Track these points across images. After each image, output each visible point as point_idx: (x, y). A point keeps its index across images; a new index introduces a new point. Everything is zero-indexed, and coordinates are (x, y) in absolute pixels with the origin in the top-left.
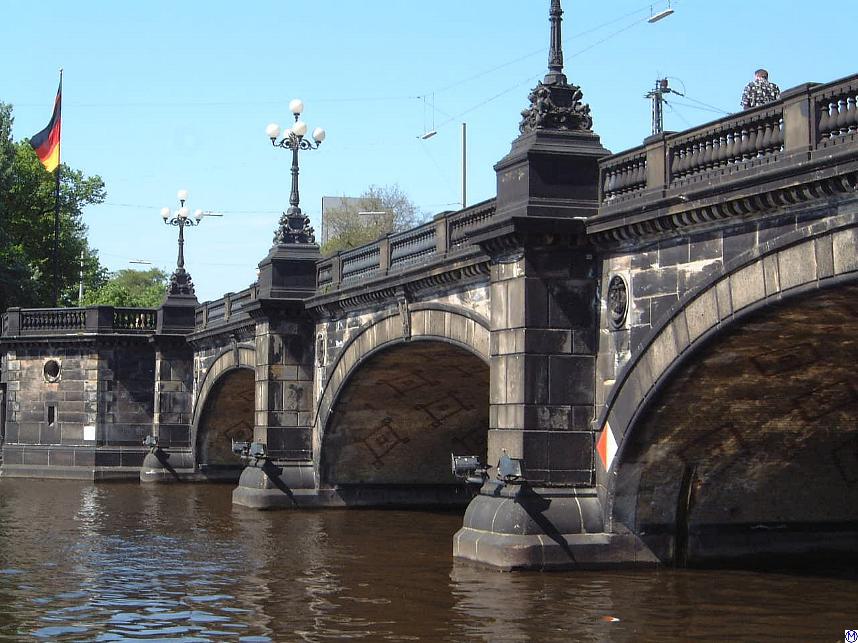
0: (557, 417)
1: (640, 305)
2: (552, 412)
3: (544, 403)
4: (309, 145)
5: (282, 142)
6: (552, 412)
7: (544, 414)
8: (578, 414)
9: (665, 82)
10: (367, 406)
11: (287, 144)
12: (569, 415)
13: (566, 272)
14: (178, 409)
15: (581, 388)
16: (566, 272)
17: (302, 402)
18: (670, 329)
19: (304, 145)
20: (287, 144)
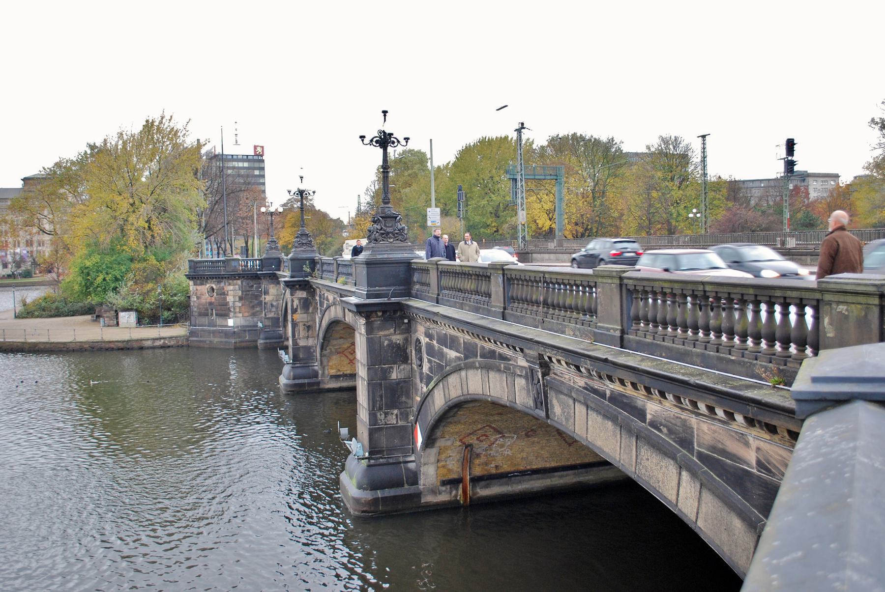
0: (389, 417)
1: (430, 361)
2: (386, 414)
3: (380, 409)
4: (398, 142)
5: (372, 141)
6: (386, 414)
7: (381, 416)
8: (401, 414)
9: (522, 124)
10: (341, 338)
11: (377, 142)
12: (397, 415)
13: (392, 330)
14: (274, 309)
15: (404, 399)
16: (392, 330)
17: (310, 332)
18: (441, 384)
19: (393, 143)
20: (377, 142)
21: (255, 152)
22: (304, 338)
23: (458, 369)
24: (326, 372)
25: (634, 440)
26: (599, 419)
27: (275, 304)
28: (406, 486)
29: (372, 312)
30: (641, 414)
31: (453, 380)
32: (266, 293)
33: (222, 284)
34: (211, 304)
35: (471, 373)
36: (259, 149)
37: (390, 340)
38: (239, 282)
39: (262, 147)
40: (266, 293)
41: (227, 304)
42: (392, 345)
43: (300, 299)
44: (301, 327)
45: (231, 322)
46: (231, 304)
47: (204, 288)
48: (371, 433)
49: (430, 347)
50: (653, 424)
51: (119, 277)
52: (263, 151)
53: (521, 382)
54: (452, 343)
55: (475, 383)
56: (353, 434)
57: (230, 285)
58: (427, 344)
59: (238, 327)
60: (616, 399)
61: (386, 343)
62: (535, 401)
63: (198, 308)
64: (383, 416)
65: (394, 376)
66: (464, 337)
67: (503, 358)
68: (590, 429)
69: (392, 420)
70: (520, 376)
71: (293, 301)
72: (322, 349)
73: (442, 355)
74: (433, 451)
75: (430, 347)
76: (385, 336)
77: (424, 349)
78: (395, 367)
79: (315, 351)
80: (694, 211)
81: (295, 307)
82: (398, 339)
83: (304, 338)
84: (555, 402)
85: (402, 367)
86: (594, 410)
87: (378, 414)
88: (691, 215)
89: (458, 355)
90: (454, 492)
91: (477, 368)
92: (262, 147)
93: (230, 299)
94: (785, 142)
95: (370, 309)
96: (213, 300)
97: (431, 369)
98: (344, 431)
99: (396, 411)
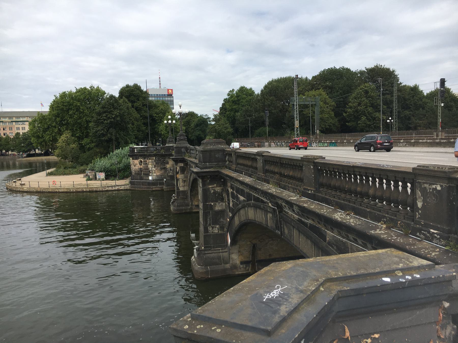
1: (233, 201)
2: (213, 228)
3: (210, 225)
7: (210, 229)
13: (215, 185)
15: (222, 220)
17: (185, 184)
21: (168, 92)
22: (182, 186)
23: (244, 207)
24: (193, 203)
25: (321, 251)
26: (305, 238)
27: (172, 168)
28: (223, 265)
29: (205, 176)
30: (323, 237)
31: (242, 212)
32: (168, 163)
33: (146, 160)
34: (141, 169)
35: (249, 209)
36: (170, 91)
37: (214, 190)
38: (154, 158)
39: (172, 90)
40: (168, 163)
41: (148, 169)
42: (215, 192)
43: (180, 167)
44: (181, 181)
45: (150, 178)
46: (150, 169)
47: (137, 162)
48: (205, 237)
49: (232, 193)
50: (329, 243)
51: (79, 160)
52: (172, 92)
53: (269, 215)
54: (242, 193)
55: (251, 214)
56: (197, 238)
57: (150, 159)
58: (232, 192)
59: (154, 180)
60: (312, 228)
61: (212, 191)
62: (276, 225)
63: (135, 171)
64: (211, 228)
65: (217, 209)
66: (247, 190)
67: (262, 201)
68: (301, 243)
69: (216, 231)
70: (270, 212)
71: (176, 168)
72: (191, 191)
73: (238, 198)
74: (237, 247)
75: (232, 193)
76: (212, 188)
77: (230, 195)
78: (217, 204)
79: (188, 193)
80: (390, 118)
81: (178, 171)
82: (218, 189)
83: (182, 186)
84: (285, 227)
85: (221, 204)
86: (302, 233)
87: (209, 228)
88: (388, 121)
89: (244, 199)
90: (248, 268)
91: (252, 207)
92: (172, 90)
93: (150, 166)
94: (439, 80)
95: (204, 174)
96: (142, 167)
97: (233, 205)
98: (193, 235)
99: (218, 226)
